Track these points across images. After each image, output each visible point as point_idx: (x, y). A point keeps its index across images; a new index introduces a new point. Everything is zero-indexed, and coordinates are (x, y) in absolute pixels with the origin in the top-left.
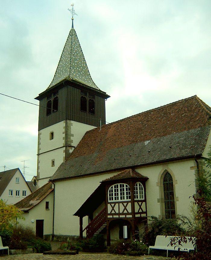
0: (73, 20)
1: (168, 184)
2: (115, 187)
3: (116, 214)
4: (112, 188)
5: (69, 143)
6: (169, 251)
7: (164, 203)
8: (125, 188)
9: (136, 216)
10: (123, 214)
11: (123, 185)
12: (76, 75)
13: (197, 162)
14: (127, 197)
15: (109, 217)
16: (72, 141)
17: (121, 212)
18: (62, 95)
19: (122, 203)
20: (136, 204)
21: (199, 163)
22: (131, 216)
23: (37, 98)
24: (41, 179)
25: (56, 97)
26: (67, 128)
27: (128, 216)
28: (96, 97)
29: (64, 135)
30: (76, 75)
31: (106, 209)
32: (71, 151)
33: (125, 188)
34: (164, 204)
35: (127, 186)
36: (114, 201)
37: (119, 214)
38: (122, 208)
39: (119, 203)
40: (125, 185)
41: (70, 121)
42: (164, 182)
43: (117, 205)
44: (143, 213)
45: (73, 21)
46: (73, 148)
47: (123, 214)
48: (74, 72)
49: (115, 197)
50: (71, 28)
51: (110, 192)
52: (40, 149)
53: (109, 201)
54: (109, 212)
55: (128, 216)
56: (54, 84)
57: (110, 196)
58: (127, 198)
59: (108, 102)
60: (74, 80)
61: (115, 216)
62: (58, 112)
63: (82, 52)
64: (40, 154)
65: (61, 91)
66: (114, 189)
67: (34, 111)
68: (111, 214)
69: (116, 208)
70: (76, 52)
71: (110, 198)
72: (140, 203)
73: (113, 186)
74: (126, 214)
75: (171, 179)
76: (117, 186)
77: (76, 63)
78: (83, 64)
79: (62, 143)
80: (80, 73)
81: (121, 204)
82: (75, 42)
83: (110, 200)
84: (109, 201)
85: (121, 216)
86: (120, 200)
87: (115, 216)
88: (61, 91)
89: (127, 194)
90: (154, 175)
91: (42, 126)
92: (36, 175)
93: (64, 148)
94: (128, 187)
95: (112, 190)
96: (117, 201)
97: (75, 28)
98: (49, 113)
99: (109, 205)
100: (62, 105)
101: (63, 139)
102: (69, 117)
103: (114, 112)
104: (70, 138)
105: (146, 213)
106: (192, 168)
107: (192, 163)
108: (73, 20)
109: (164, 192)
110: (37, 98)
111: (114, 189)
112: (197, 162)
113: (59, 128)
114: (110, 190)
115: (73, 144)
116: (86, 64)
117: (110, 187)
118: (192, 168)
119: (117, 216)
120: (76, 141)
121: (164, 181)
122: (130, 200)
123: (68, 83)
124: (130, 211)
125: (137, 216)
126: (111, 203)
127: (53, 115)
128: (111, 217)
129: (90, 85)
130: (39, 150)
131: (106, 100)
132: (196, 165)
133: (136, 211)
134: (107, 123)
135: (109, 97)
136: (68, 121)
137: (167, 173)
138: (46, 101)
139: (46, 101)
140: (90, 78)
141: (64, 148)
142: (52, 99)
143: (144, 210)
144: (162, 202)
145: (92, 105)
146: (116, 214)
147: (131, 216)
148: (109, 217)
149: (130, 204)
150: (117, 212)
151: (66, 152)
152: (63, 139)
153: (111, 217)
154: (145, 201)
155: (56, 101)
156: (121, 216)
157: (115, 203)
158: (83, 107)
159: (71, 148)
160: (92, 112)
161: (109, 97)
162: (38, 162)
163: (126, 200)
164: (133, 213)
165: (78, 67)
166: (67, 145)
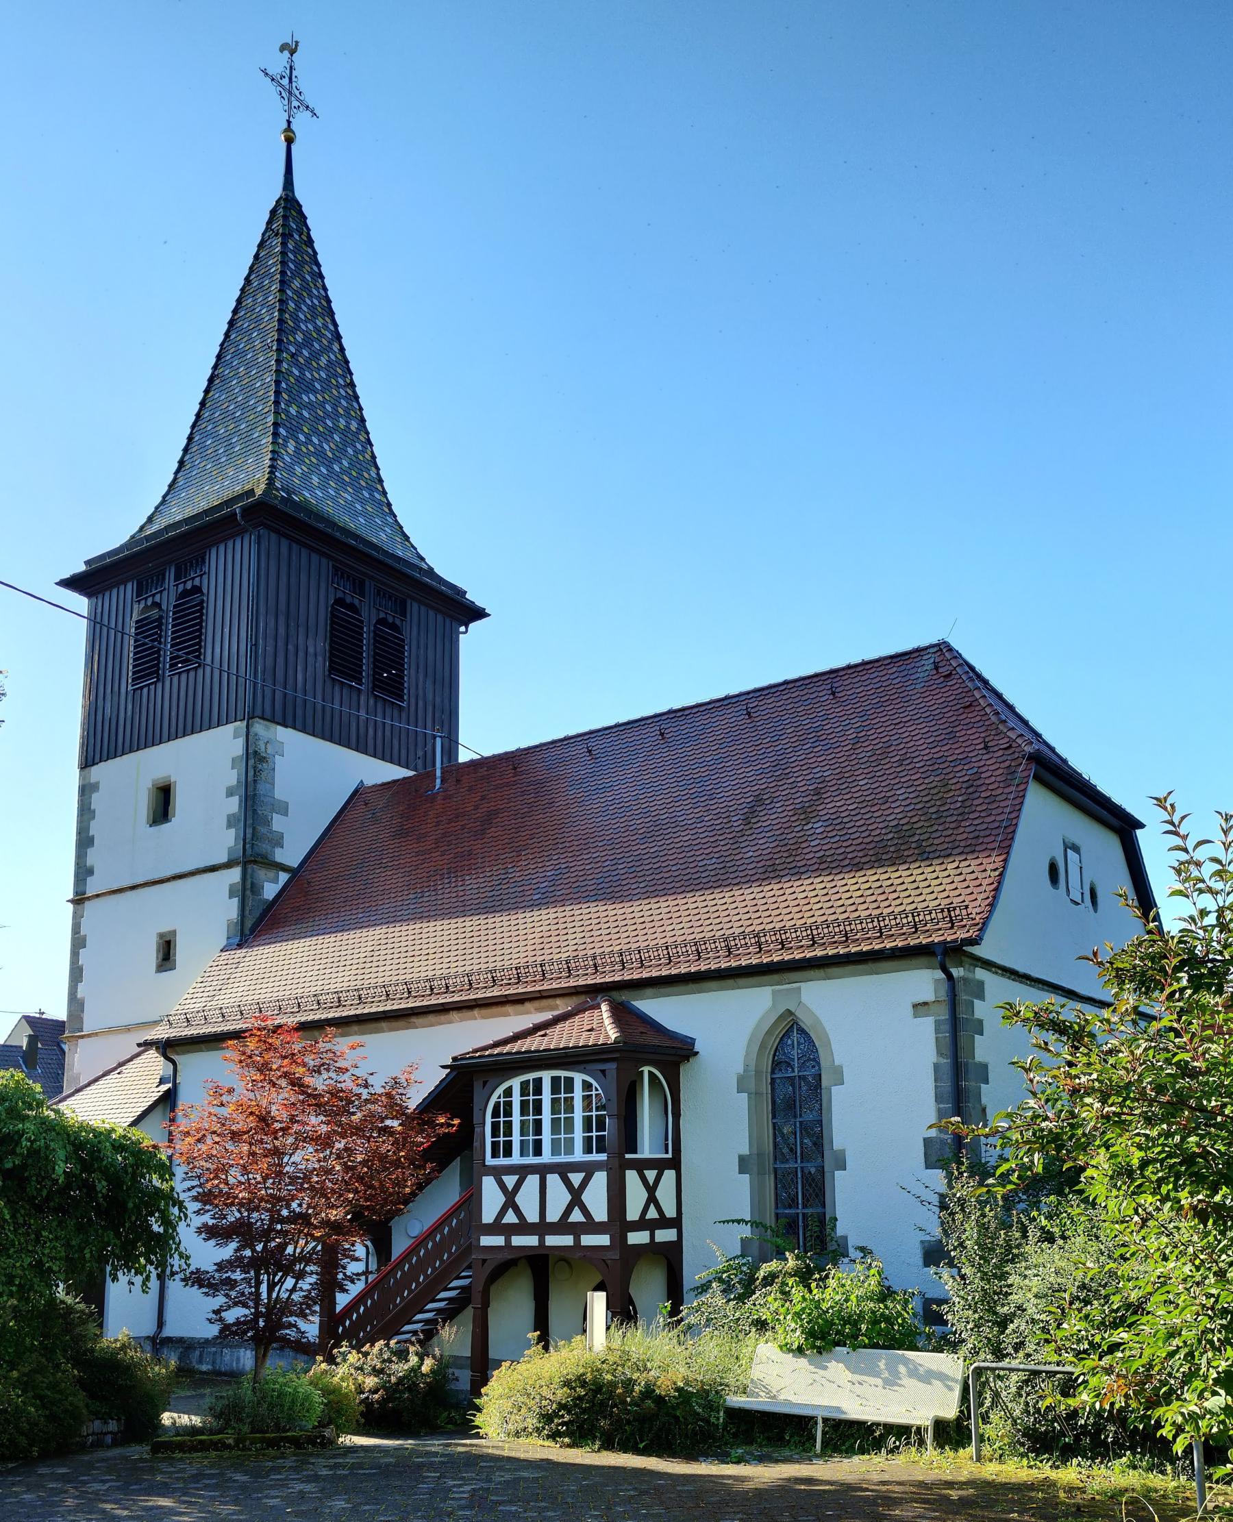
0: (290, 141)
1: (793, 1083)
2: (524, 1091)
3: (523, 1227)
4: (508, 1093)
5: (264, 847)
6: (825, 1420)
7: (772, 1176)
8: (578, 1094)
9: (630, 1242)
10: (563, 1226)
11: (570, 1082)
12: (305, 477)
13: (950, 976)
14: (588, 1141)
15: (486, 1241)
16: (278, 841)
17: (553, 1216)
18: (230, 576)
19: (563, 1170)
20: (631, 1176)
21: (960, 986)
22: (604, 1240)
23: (72, 583)
24: (89, 1036)
25: (194, 587)
26: (255, 764)
27: (588, 1240)
28: (414, 608)
29: (233, 805)
30: (305, 477)
31: (471, 1200)
32: (270, 891)
33: (578, 1094)
34: (770, 1182)
35: (587, 1086)
36: (516, 1159)
37: (543, 1228)
38: (558, 1197)
39: (543, 1171)
40: (578, 1078)
41: (273, 725)
42: (773, 1072)
43: (533, 1181)
44: (664, 1222)
45: (293, 147)
46: (284, 877)
47: (563, 1226)
48: (298, 456)
49: (522, 1141)
50: (277, 191)
51: (496, 1114)
52: (90, 872)
53: (490, 1161)
54: (488, 1216)
55: (588, 1240)
56: (177, 513)
57: (495, 1133)
58: (588, 1150)
59: (472, 642)
60: (294, 502)
61: (517, 1241)
62: (200, 671)
63: (342, 349)
64: (88, 898)
65: (230, 551)
66: (516, 1099)
67: (52, 655)
68: (497, 1227)
69: (528, 1200)
70: (308, 342)
71: (495, 1145)
72: (651, 1175)
73: (515, 1083)
74: (576, 1230)
75: (811, 1055)
76: (538, 1082)
77: (310, 406)
78: (348, 416)
79: (224, 843)
80: (329, 468)
81: (553, 1180)
82: (303, 279)
83: (495, 1155)
84: (490, 1161)
85: (552, 1240)
86: (547, 1157)
87: (517, 1241)
88: (230, 551)
89: (587, 1126)
90: (723, 1030)
91: (103, 741)
92: (58, 1011)
93: (235, 875)
94: (597, 1089)
95: (509, 1105)
96: (531, 1160)
97: (300, 194)
98: (148, 668)
99: (489, 1183)
100: (227, 636)
101: (229, 826)
102: (278, 703)
103: (503, 704)
104: (268, 823)
105: (676, 1223)
106: (920, 1008)
107: (923, 982)
108: (290, 141)
109: (774, 1124)
110: (72, 583)
111: (516, 1099)
112: (950, 976)
113: (203, 762)
114: (497, 1105)
115: (280, 856)
116: (363, 420)
117: (500, 1090)
118: (920, 1008)
119: (532, 1241)
120: (295, 841)
121: (776, 1065)
122: (603, 1157)
123: (270, 518)
124: (600, 1213)
125: (637, 1238)
126: (498, 1173)
127: (169, 690)
128: (499, 1241)
129: (381, 537)
130: (83, 872)
131: (462, 629)
132: (943, 995)
133: (633, 1214)
134: (464, 756)
135: (479, 614)
136: (259, 727)
137: (787, 1034)
138: (129, 608)
139: (129, 608)
140: (380, 503)
141: (235, 875)
142: (168, 596)
143: (670, 1212)
144: (761, 1173)
145: (390, 655)
146: (523, 1227)
147: (604, 1240)
148: (486, 1241)
149: (600, 1178)
150: (532, 1217)
151: (246, 891)
152: (229, 826)
153: (499, 1241)
154: (675, 1163)
155: (192, 613)
156: (552, 1240)
157: (522, 1172)
158: (343, 664)
159: (271, 874)
160: (390, 688)
161: (479, 614)
162: (78, 943)
163: (579, 1155)
164: (618, 1222)
165: (315, 431)
166: (253, 855)
